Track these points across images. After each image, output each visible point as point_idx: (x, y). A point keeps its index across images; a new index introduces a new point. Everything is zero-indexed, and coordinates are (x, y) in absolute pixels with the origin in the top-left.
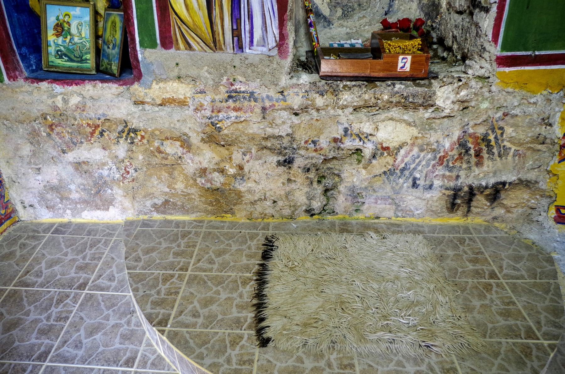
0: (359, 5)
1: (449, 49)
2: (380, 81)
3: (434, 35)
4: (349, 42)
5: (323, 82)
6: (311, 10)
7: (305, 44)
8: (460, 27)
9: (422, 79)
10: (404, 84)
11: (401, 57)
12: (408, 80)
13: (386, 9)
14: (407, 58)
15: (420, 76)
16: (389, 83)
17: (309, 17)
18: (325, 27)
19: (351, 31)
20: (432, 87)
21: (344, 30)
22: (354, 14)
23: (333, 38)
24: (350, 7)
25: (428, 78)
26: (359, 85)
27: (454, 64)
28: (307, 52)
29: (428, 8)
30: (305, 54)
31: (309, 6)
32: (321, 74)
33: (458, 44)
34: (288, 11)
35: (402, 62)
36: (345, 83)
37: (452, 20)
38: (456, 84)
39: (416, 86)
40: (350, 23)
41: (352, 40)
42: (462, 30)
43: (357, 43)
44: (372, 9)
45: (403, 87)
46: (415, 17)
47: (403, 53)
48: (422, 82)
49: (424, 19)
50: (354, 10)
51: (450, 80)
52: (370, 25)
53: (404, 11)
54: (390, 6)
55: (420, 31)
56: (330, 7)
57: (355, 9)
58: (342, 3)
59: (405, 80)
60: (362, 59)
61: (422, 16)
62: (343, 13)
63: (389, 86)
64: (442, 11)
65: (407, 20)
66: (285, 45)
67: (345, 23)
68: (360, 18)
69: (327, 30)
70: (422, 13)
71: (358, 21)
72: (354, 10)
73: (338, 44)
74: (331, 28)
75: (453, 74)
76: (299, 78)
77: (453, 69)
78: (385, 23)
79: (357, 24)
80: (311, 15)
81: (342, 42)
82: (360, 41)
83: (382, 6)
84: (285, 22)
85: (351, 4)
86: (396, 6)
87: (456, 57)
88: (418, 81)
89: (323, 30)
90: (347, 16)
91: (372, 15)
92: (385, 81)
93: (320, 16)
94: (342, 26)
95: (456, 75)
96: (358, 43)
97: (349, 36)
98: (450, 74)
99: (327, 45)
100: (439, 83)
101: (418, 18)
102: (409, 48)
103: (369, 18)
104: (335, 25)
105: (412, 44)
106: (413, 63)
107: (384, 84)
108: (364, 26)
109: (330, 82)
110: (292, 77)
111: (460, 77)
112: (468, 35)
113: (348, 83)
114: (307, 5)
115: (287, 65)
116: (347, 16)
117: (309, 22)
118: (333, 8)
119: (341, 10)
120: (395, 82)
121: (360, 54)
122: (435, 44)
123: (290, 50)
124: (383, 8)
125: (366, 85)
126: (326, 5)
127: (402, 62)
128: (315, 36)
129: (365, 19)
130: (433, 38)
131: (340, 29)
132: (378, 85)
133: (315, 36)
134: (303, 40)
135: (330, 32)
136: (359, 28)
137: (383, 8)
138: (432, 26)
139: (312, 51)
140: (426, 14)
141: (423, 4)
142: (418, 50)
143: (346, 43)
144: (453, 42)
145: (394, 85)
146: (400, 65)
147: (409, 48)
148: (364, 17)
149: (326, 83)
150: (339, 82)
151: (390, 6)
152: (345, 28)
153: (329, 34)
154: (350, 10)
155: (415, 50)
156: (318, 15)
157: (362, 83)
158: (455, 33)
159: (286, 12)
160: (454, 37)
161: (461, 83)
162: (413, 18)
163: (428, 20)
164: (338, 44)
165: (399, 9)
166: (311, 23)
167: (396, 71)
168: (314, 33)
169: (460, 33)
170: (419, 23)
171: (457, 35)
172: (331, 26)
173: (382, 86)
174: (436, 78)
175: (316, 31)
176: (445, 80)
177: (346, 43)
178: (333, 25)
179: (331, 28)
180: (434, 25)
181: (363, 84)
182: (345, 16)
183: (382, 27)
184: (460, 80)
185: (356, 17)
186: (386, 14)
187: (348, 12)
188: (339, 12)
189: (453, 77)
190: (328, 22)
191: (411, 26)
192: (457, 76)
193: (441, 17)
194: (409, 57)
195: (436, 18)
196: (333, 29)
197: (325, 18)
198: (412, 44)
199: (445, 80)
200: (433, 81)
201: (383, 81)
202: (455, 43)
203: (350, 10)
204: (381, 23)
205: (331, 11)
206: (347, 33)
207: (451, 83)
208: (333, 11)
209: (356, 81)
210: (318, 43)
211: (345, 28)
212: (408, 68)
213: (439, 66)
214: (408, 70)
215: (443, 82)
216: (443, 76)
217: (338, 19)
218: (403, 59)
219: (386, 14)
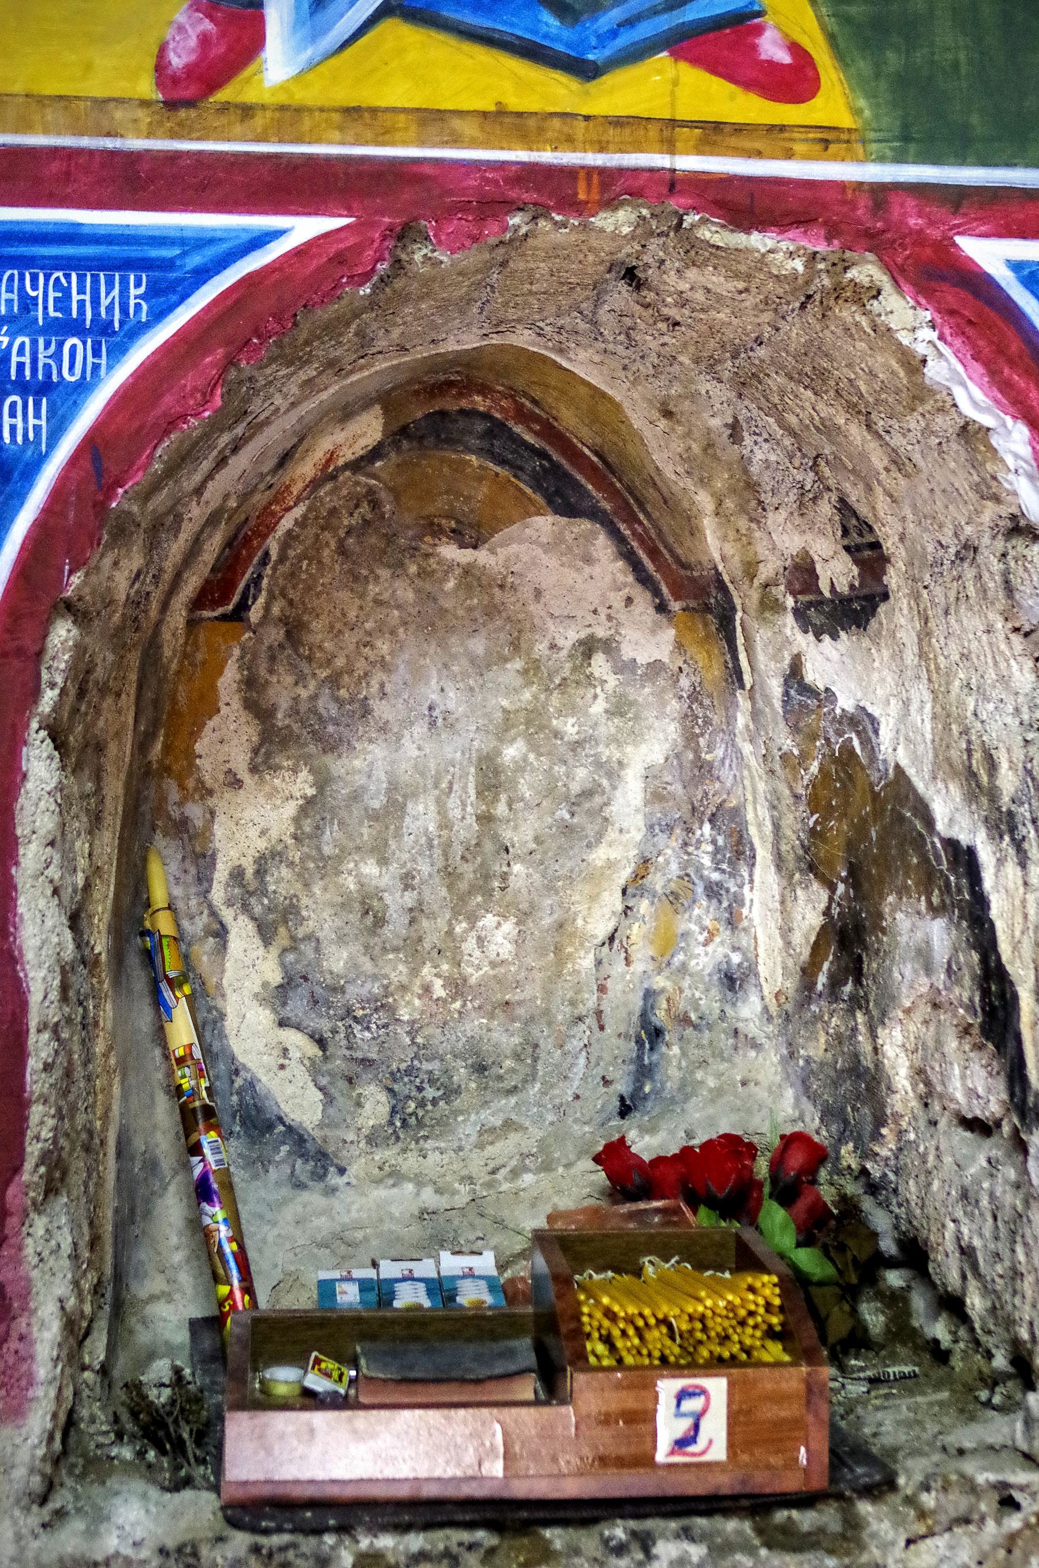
0: (480, 1069)
1: (952, 1305)
2: (564, 1523)
3: (880, 1221)
4: (425, 1269)
5: (240, 1541)
6: (209, 1112)
7: (185, 1278)
8: (985, 1202)
9: (805, 1501)
10: (703, 1538)
11: (667, 1387)
12: (726, 1513)
13: (623, 1086)
14: (703, 1392)
15: (791, 1483)
16: (619, 1531)
17: (196, 1149)
18: (300, 1186)
19: (440, 1202)
20: (862, 1547)
21: (403, 1200)
22: (456, 1113)
23: (340, 1243)
24: (432, 1082)
25: (840, 1497)
26: (447, 1554)
27: (984, 1395)
28: (195, 1326)
29: (835, 1084)
30: (182, 1337)
31: (194, 1093)
32: (229, 1493)
33: (987, 1290)
34: (28, 1165)
35: (679, 1415)
36: (365, 1543)
37: (948, 1160)
38: (990, 1525)
39: (769, 1545)
40: (434, 1158)
41: (445, 1256)
42: (995, 1218)
43: (470, 1274)
44: (548, 1087)
45: (697, 1552)
46: (775, 1126)
47: (691, 1366)
48: (805, 1520)
49: (822, 1137)
50: (451, 1092)
51: (957, 1502)
52: (547, 1167)
53: (718, 1093)
54: (643, 1072)
55: (802, 1204)
56: (324, 1081)
57: (457, 1091)
58: (386, 1062)
59: (708, 1513)
60: (478, 1381)
61: (812, 1124)
62: (393, 1111)
63: (620, 1550)
64: (899, 1108)
65: (734, 1148)
66: (13, 1344)
67: (410, 1163)
68: (488, 1134)
69: (313, 1198)
70: (807, 1106)
71: (481, 1146)
72: (451, 1092)
73: (365, 1286)
74: (334, 1190)
75: (969, 1467)
76: (99, 1518)
77: (967, 1436)
78: (613, 1156)
79: (476, 1164)
80: (208, 1139)
81: (389, 1270)
82: (486, 1263)
83: (599, 1071)
84: (12, 1222)
85: (435, 1066)
86: (674, 1072)
87: (989, 1356)
88: (781, 1516)
89: (285, 1202)
90: (420, 1123)
91: (550, 1117)
92: (595, 1521)
93: (270, 1127)
94: (396, 1176)
95: (984, 1478)
96: (474, 1272)
97: (437, 1232)
98: (953, 1468)
99: (302, 1300)
100: (899, 1522)
101: (788, 1130)
102: (717, 1326)
103: (536, 1133)
104: (353, 1170)
105: (731, 1307)
106: (735, 1419)
107: (588, 1541)
108: (515, 1174)
109: (277, 1540)
110: (60, 1514)
111: (1004, 1485)
112: (1019, 1249)
113: (386, 1542)
114: (186, 1084)
115: (24, 1456)
116: (420, 1123)
117: (198, 1171)
118: (342, 1084)
119: (383, 1097)
120: (650, 1524)
121: (471, 1349)
122: (892, 1263)
123: (43, 1370)
124: (606, 1082)
125: (491, 1551)
126: (300, 1073)
127: (679, 1415)
128: (230, 1248)
129: (514, 1137)
130: (875, 1235)
131: (380, 1193)
132: (558, 1545)
133: (230, 1248)
134: (178, 1257)
135: (327, 1212)
136: (489, 1185)
137: (606, 1082)
138: (864, 1172)
139: (214, 1323)
140: (828, 1114)
141: (808, 1060)
142: (770, 1334)
143: (409, 1278)
144: (964, 1277)
145: (645, 1542)
146: (668, 1427)
147: (717, 1326)
148: (509, 1125)
149: (256, 1549)
150: (329, 1539)
151: (643, 1072)
152: (409, 1187)
153: (322, 1222)
154: (430, 1093)
155: (750, 1337)
156: (259, 1122)
157: (465, 1536)
158: (965, 1230)
159: (17, 1169)
160: (967, 1252)
161: (1014, 1522)
162: (765, 1128)
163: (840, 1141)
164: (365, 1286)
165: (687, 1089)
166: (204, 1178)
167: (646, 1460)
168: (224, 1232)
169: (987, 1232)
170: (796, 1159)
171: (977, 1242)
172: (334, 1179)
173: (577, 1552)
174: (882, 1487)
175: (234, 1220)
176: (928, 1500)
177: (409, 1278)
178: (342, 1171)
179: (334, 1190)
180: (875, 1170)
181: (471, 1547)
182: (407, 1123)
183: (601, 1177)
184: (1009, 1503)
185: (467, 1129)
186: (625, 1111)
187: (422, 1104)
188: (375, 1105)
189: (971, 1487)
190: (317, 1159)
191: (762, 1167)
192: (992, 1477)
193: (900, 1133)
194: (717, 1386)
195: (876, 1136)
196: (347, 1196)
197: (297, 1137)
198: (731, 1307)
199: (928, 1500)
200: (865, 1508)
201: (586, 1523)
202: (973, 1284)
203: (430, 1093)
204: (597, 1159)
205: (329, 1100)
206: (425, 1214)
207: (967, 1521)
208: (340, 1101)
209: (428, 1526)
210: (248, 1289)
211: (409, 1187)
212: (714, 1441)
213: (903, 1407)
214: (719, 1453)
215: (922, 1515)
216: (919, 1477)
217: (370, 1140)
218: (682, 1396)
219: (625, 1111)
